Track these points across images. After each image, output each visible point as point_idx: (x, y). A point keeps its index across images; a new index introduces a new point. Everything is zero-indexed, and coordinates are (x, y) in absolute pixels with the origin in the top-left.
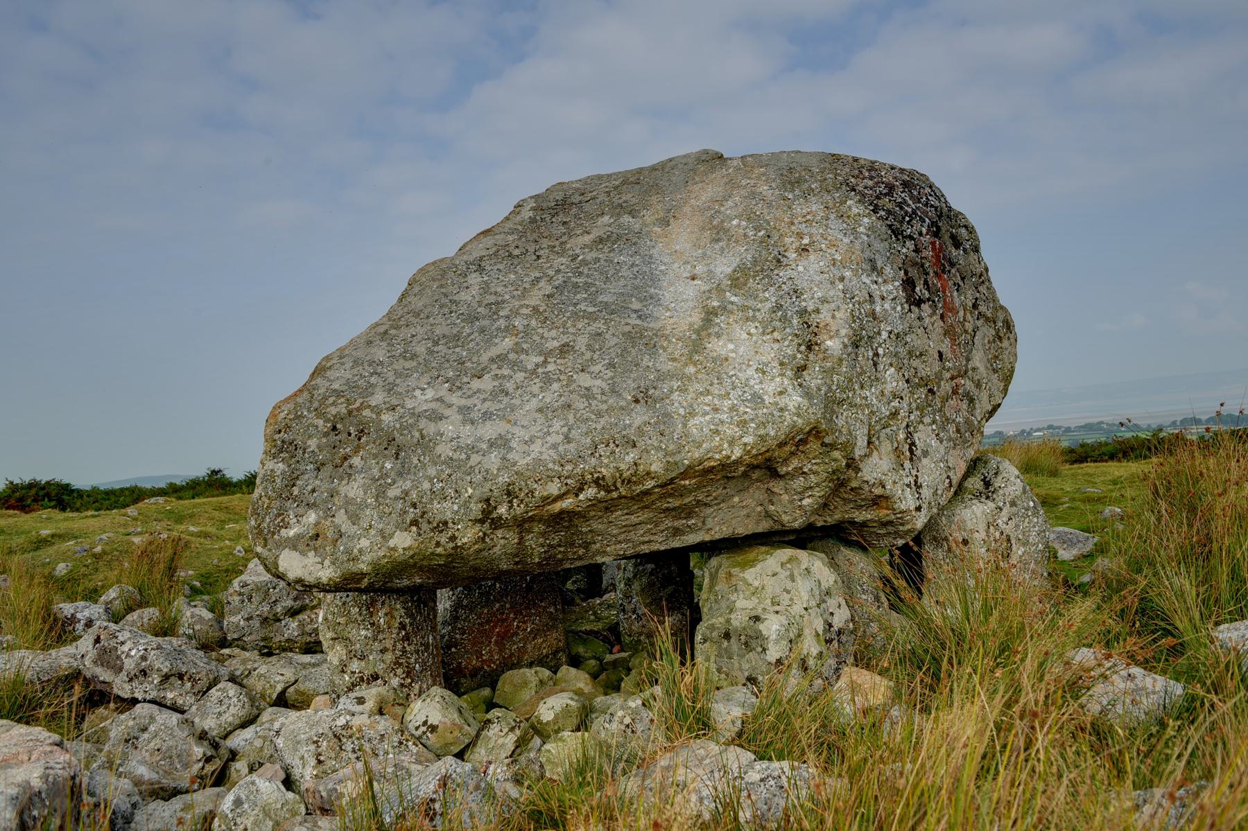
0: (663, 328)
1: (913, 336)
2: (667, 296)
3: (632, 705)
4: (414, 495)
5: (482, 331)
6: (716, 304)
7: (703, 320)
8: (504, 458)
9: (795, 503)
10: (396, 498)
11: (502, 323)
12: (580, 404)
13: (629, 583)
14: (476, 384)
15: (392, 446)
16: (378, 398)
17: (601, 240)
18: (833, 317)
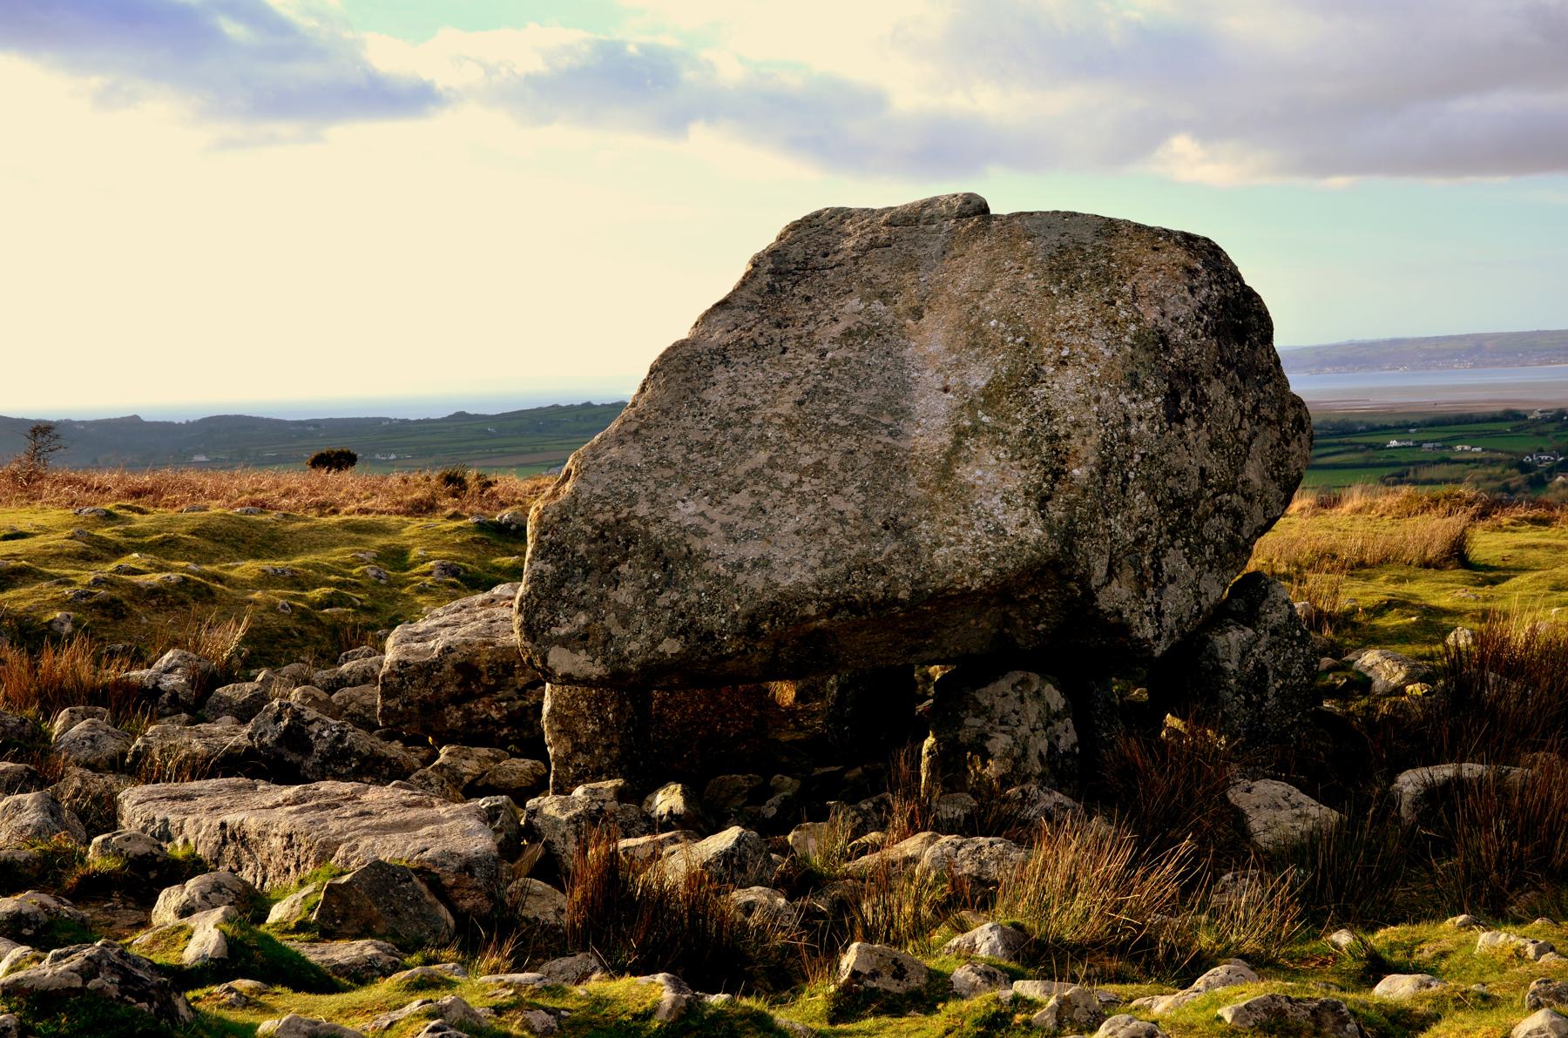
0: (913, 449)
1: (1172, 455)
2: (919, 407)
3: (864, 807)
4: (682, 605)
5: (735, 440)
6: (967, 423)
7: (953, 442)
8: (767, 579)
10: (666, 608)
11: (754, 432)
12: (835, 530)
14: (735, 500)
16: (642, 509)
17: (848, 333)
18: (1084, 443)
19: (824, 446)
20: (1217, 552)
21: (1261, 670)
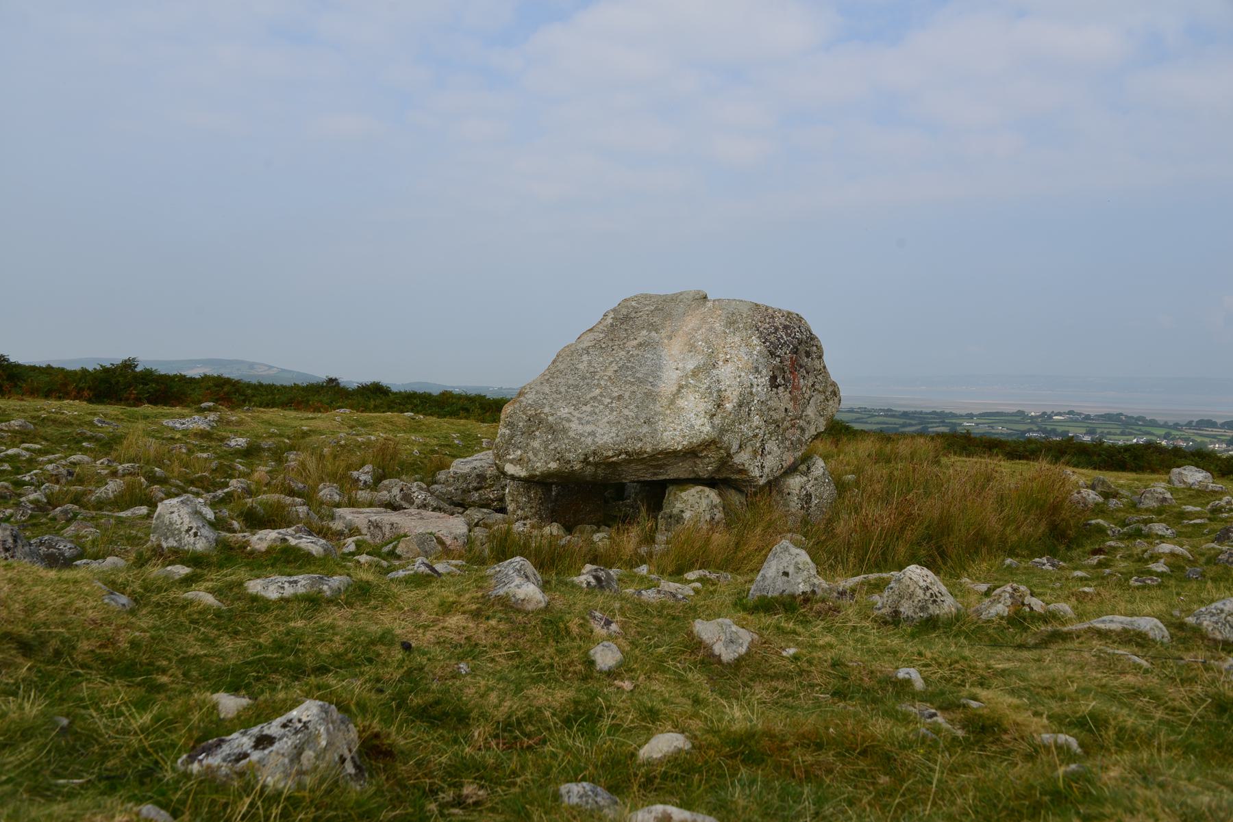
2: (665, 377)
9: (706, 468)
12: (624, 422)
13: (637, 494)
14: (584, 408)
15: (551, 429)
16: (547, 410)
17: (640, 345)
21: (809, 495)
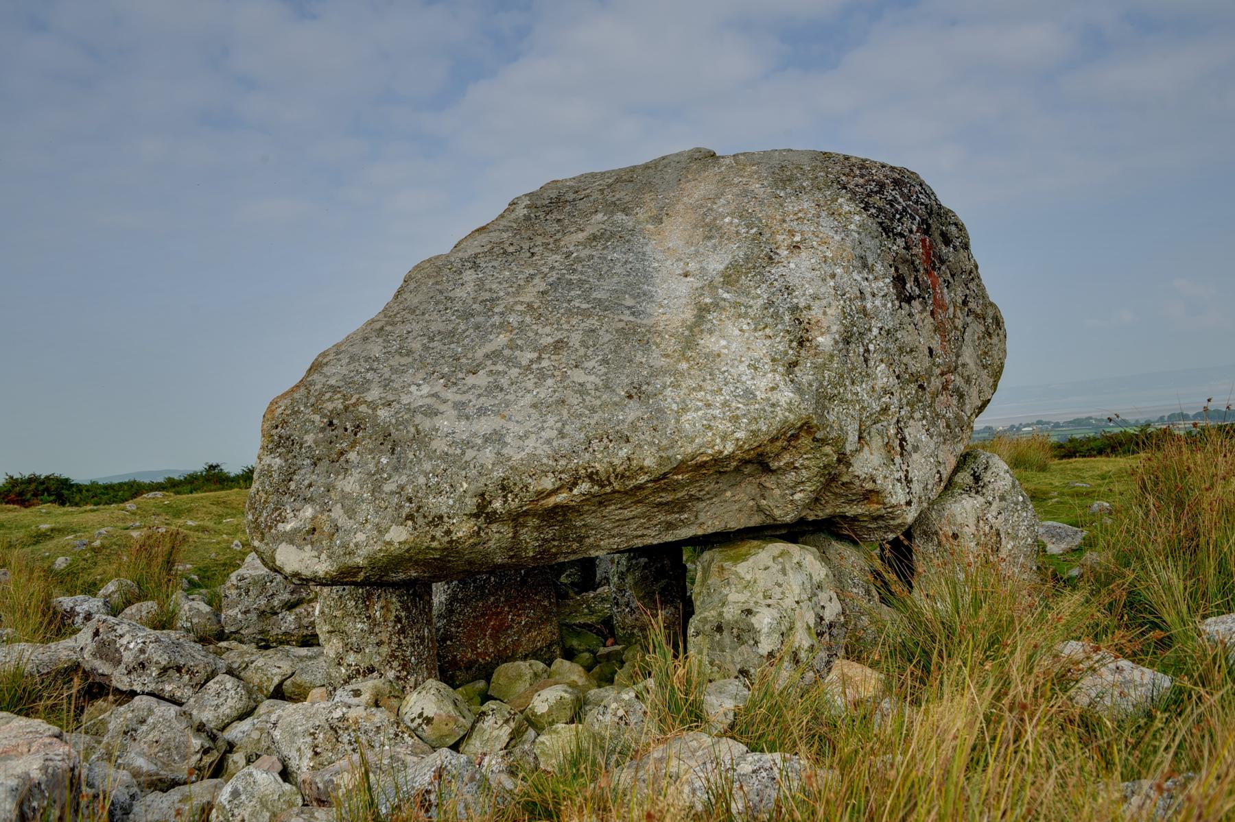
2: (660, 293)
4: (409, 490)
5: (477, 327)
6: (708, 300)
8: (498, 453)
9: (787, 498)
10: (392, 493)
11: (497, 319)
12: (574, 400)
13: (622, 576)
14: (471, 380)
15: (388, 440)
16: (374, 394)
17: (594, 238)
18: (825, 313)
19: (565, 326)
20: (948, 426)
